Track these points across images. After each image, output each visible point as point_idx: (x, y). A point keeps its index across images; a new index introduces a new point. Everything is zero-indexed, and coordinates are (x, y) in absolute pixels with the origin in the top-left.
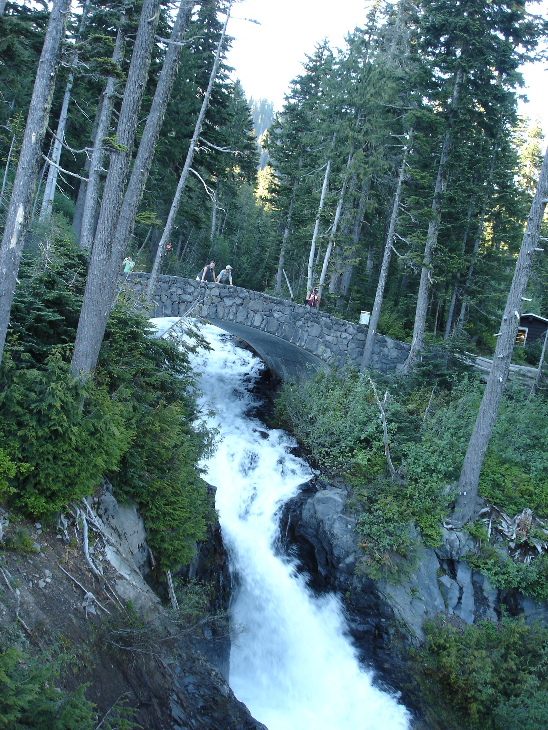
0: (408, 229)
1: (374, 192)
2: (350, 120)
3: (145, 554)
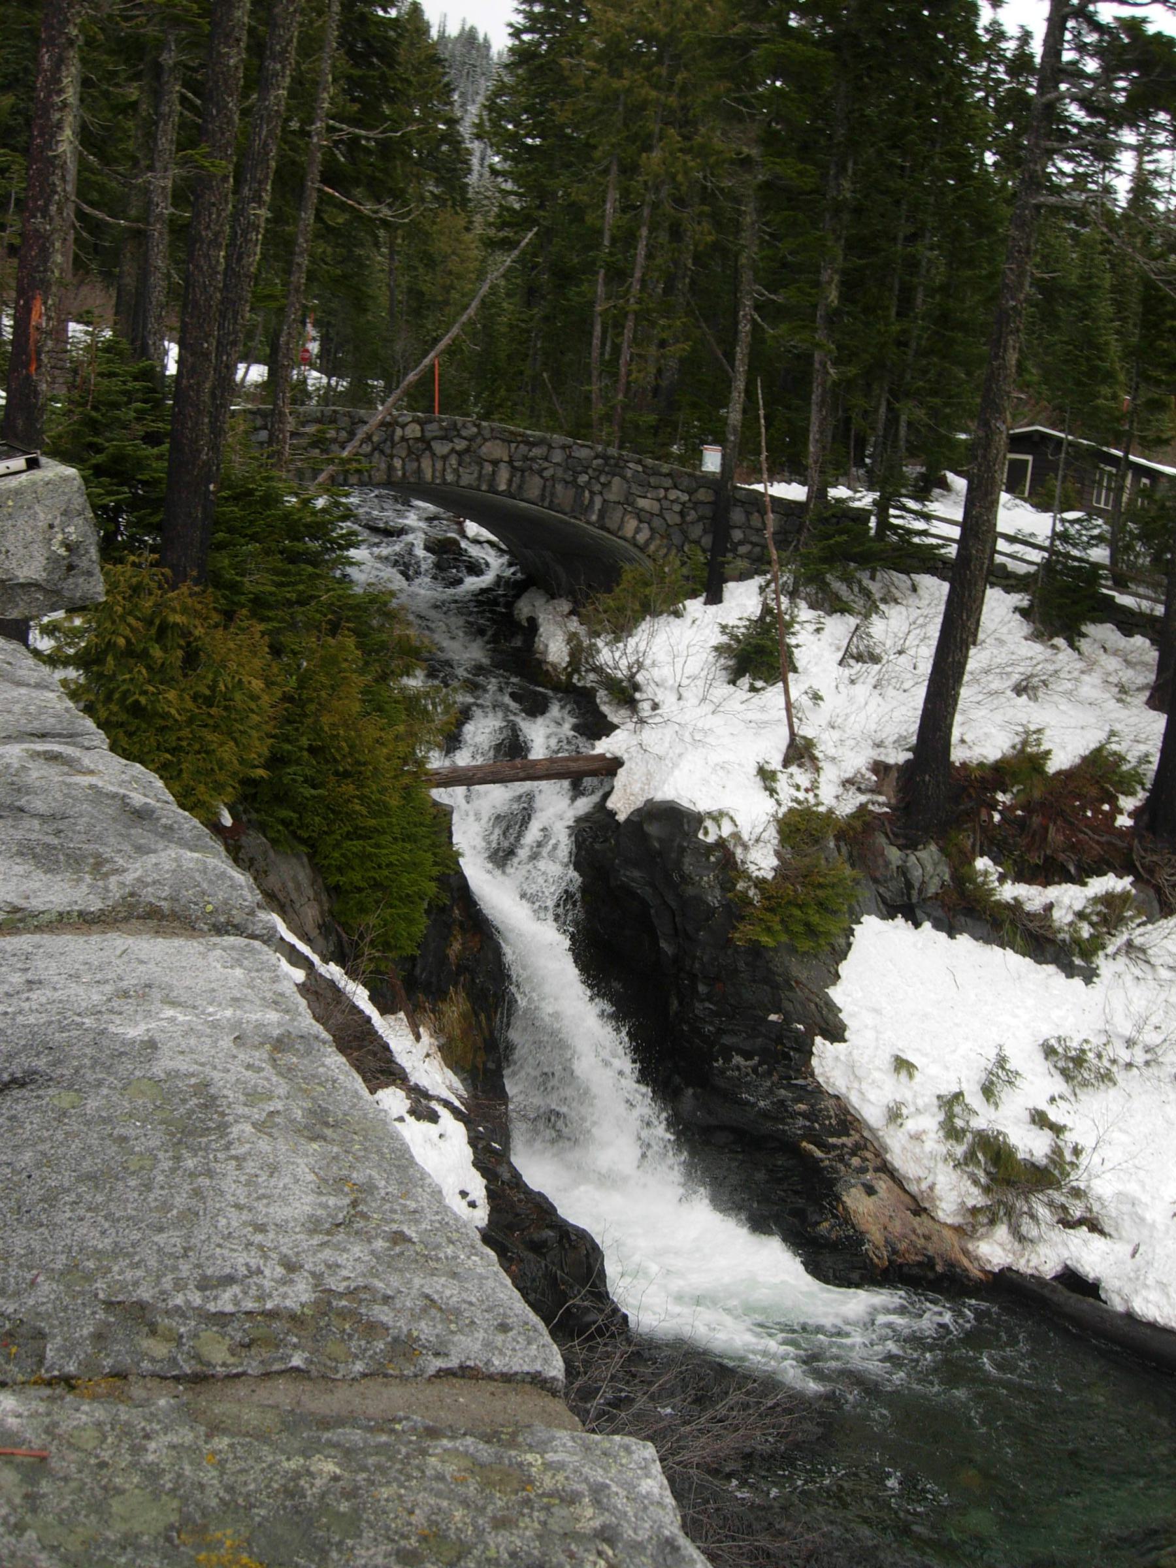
0: (779, 273)
1: (706, 208)
2: (648, 68)
3: (333, 938)
